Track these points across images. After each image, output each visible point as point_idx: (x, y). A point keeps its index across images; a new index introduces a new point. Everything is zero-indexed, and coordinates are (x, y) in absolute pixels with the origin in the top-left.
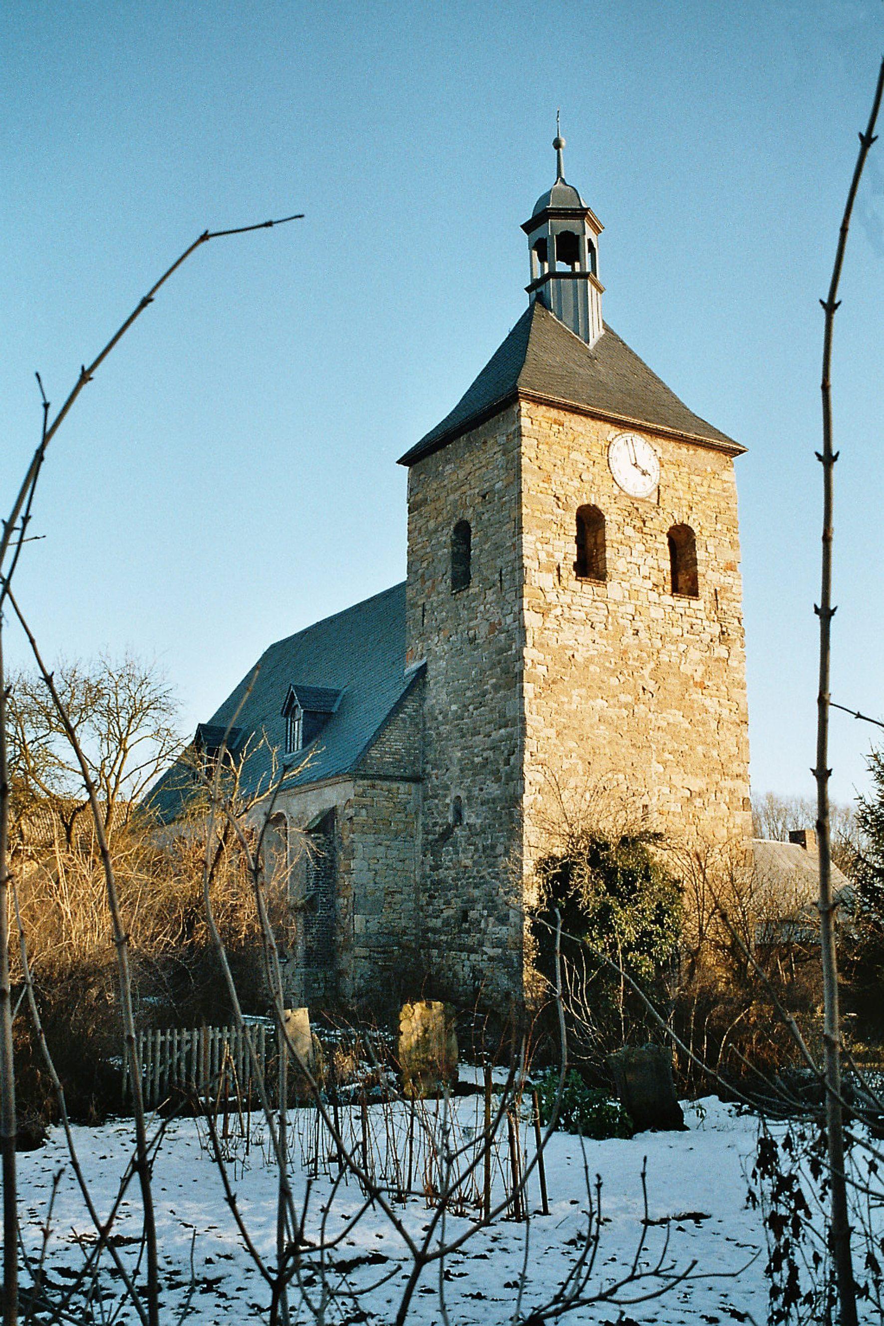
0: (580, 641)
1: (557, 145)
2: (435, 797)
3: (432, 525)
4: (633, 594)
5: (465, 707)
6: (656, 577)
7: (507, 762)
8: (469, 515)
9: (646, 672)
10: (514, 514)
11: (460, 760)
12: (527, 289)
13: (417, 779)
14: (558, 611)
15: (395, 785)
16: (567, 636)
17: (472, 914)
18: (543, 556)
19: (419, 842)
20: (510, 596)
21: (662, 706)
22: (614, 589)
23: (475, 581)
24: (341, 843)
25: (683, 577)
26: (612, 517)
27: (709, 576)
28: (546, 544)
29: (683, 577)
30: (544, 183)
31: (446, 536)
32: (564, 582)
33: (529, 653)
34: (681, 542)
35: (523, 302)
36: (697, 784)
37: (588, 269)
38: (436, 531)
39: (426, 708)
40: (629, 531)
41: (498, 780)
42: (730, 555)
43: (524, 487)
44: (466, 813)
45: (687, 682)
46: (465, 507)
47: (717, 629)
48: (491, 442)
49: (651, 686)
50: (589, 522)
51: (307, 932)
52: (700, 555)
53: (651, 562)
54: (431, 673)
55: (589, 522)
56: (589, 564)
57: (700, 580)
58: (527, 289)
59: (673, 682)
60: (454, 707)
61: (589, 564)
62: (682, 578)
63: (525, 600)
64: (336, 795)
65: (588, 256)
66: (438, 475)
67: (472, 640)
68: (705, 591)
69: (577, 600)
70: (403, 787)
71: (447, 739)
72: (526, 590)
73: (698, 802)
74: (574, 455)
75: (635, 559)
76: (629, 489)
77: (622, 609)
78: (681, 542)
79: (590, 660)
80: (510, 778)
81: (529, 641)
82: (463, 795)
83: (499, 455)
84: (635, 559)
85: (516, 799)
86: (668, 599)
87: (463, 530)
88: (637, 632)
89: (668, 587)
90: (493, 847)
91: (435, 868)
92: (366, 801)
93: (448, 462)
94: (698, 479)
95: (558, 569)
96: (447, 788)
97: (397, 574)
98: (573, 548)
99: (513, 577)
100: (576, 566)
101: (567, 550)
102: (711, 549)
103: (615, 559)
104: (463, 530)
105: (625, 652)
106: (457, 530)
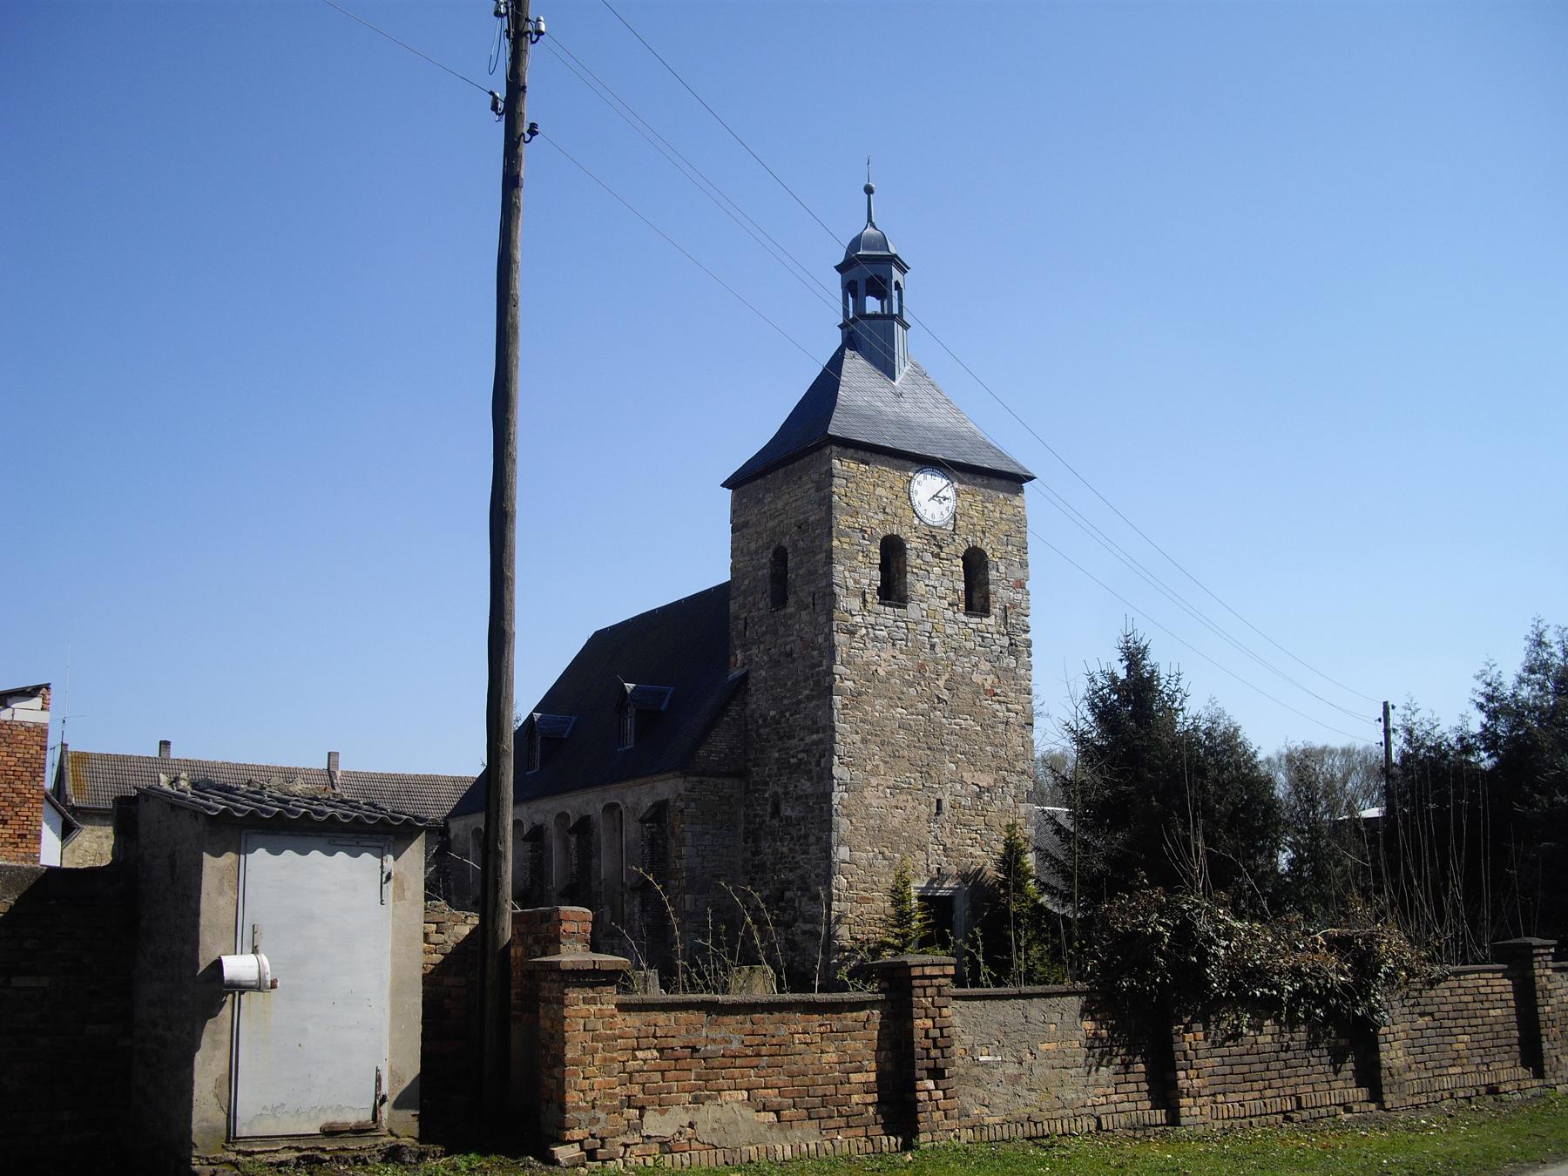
0: (882, 659)
1: (869, 190)
2: (756, 791)
3: (753, 546)
4: (931, 613)
5: (782, 713)
6: (952, 597)
7: (818, 764)
8: (786, 541)
9: (941, 683)
10: (825, 546)
11: (777, 760)
12: (838, 268)
13: (741, 774)
14: (864, 631)
15: (720, 781)
16: (870, 654)
17: (788, 894)
18: (851, 583)
19: (741, 830)
20: (822, 619)
21: (954, 714)
22: (913, 611)
23: (792, 600)
24: (673, 833)
25: (976, 599)
26: (913, 544)
27: (1000, 594)
28: (855, 573)
29: (976, 599)
30: (854, 226)
31: (767, 557)
32: (869, 606)
33: (838, 668)
34: (975, 563)
35: (836, 340)
36: (986, 780)
37: (895, 311)
38: (756, 552)
39: (748, 712)
40: (928, 557)
41: (810, 779)
42: (1019, 574)
43: (834, 523)
44: (783, 807)
45: (978, 690)
46: (784, 534)
47: (1006, 641)
48: (805, 478)
49: (945, 695)
50: (892, 550)
51: (643, 910)
52: (993, 574)
53: (946, 583)
54: (752, 681)
55: (892, 550)
56: (892, 590)
57: (992, 598)
58: (838, 268)
59: (965, 692)
60: (772, 713)
61: (892, 590)
62: (976, 595)
63: (835, 623)
64: (667, 788)
65: (895, 293)
66: (759, 502)
67: (789, 654)
68: (996, 610)
69: (880, 620)
70: (728, 782)
71: (767, 740)
72: (836, 614)
73: (986, 797)
74: (879, 491)
75: (935, 584)
76: (928, 518)
77: (921, 627)
78: (975, 563)
79: (890, 674)
80: (821, 778)
81: (838, 659)
82: (780, 790)
83: (812, 491)
84: (935, 584)
85: (827, 797)
86: (962, 617)
87: (780, 556)
88: (933, 646)
89: (962, 605)
90: (806, 837)
91: (754, 854)
92: (696, 795)
93: (768, 490)
94: (990, 506)
95: (864, 593)
96: (767, 784)
97: (722, 575)
98: (876, 574)
99: (826, 599)
100: (879, 591)
101: (871, 577)
102: (1002, 569)
103: (917, 585)
104: (780, 556)
105: (922, 666)
106: (775, 553)
